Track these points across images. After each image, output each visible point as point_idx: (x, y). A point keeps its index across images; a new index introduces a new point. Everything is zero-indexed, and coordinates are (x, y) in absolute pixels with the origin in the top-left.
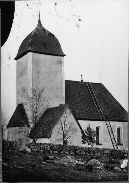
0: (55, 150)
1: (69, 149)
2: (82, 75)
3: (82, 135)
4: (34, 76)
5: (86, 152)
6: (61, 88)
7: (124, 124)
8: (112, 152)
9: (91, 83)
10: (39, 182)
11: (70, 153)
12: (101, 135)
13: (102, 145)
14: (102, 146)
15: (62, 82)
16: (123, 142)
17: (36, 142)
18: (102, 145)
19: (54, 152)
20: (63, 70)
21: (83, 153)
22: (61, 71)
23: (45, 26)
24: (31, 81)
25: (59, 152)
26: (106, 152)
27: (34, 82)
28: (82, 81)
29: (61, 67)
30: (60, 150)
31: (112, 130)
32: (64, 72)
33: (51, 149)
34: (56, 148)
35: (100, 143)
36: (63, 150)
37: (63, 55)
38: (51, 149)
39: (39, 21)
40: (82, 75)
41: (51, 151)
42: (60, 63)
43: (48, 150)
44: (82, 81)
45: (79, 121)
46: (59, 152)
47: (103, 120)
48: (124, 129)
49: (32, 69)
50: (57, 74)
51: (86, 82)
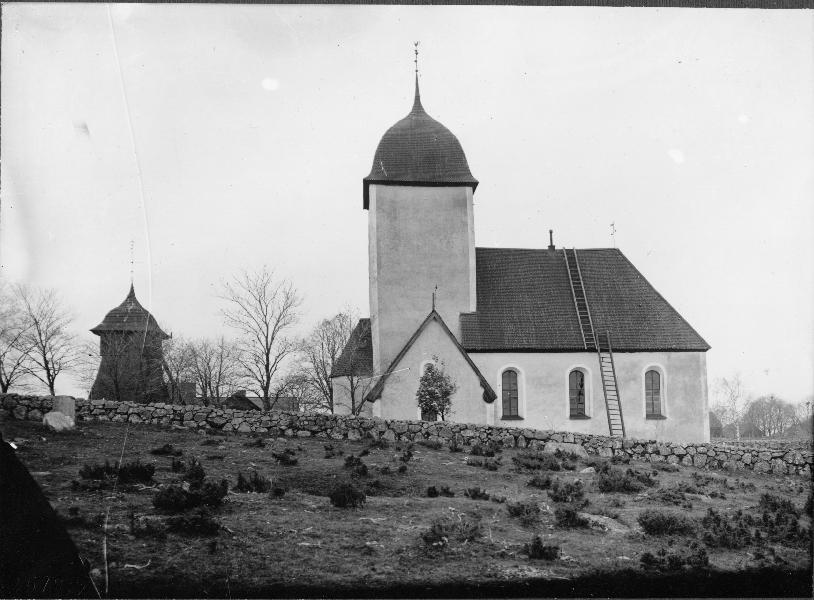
0: (304, 429)
1: (343, 426)
2: (551, 232)
3: (482, 391)
4: (383, 246)
5: (399, 435)
6: (466, 270)
7: (669, 358)
8: (490, 434)
9: (577, 250)
10: (670, 597)
11: (346, 435)
12: (589, 391)
13: (590, 418)
14: (589, 421)
15: (466, 255)
16: (667, 410)
17: (9, 391)
18: (590, 418)
19: (300, 432)
20: (469, 222)
21: (673, 461)
22: (465, 224)
23: (432, 110)
24: (375, 260)
25: (314, 433)
26: (469, 433)
27: (383, 260)
28: (552, 247)
29: (466, 213)
30: (315, 428)
31: (615, 381)
32: (473, 228)
33: (291, 426)
34: (306, 423)
35: (587, 413)
36: (326, 430)
37: (474, 185)
38: (291, 426)
39: (417, 98)
40: (551, 232)
41: (290, 432)
42: (463, 205)
43: (283, 427)
44: (552, 247)
45: (471, 355)
46: (314, 433)
47: (592, 350)
48: (669, 372)
49: (378, 228)
50: (452, 233)
51: (561, 251)
